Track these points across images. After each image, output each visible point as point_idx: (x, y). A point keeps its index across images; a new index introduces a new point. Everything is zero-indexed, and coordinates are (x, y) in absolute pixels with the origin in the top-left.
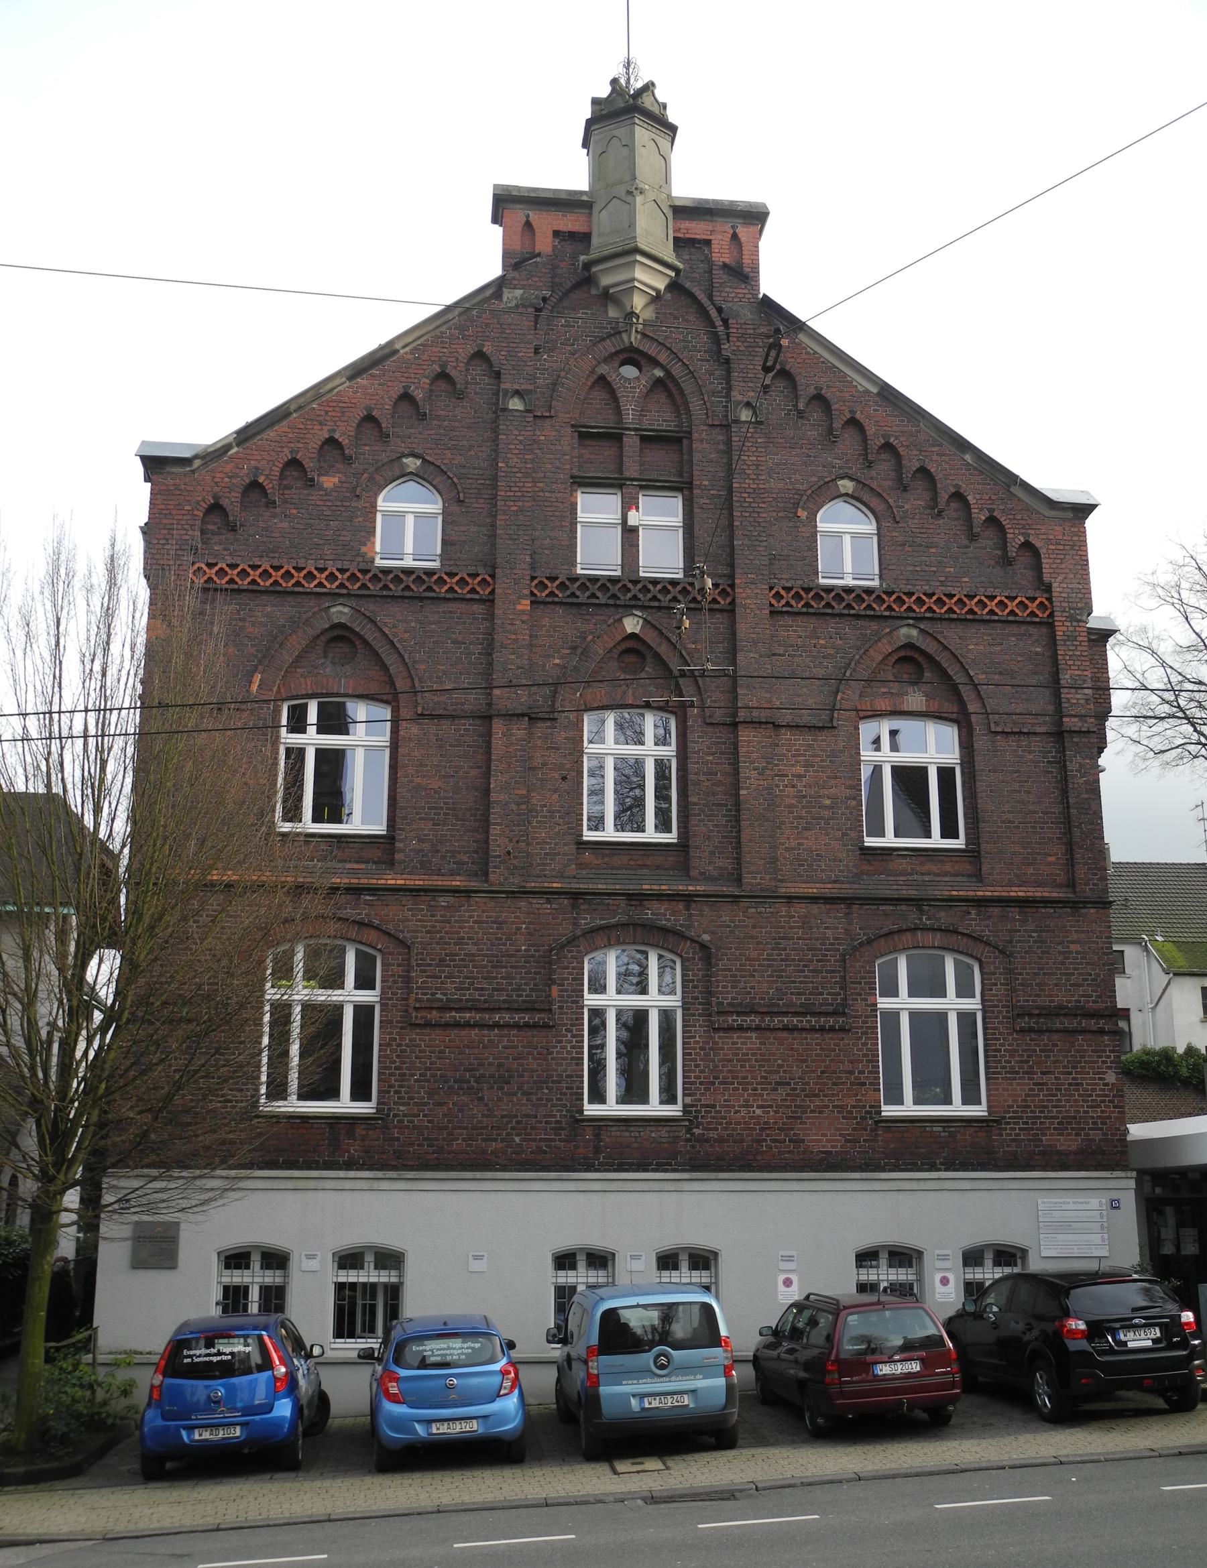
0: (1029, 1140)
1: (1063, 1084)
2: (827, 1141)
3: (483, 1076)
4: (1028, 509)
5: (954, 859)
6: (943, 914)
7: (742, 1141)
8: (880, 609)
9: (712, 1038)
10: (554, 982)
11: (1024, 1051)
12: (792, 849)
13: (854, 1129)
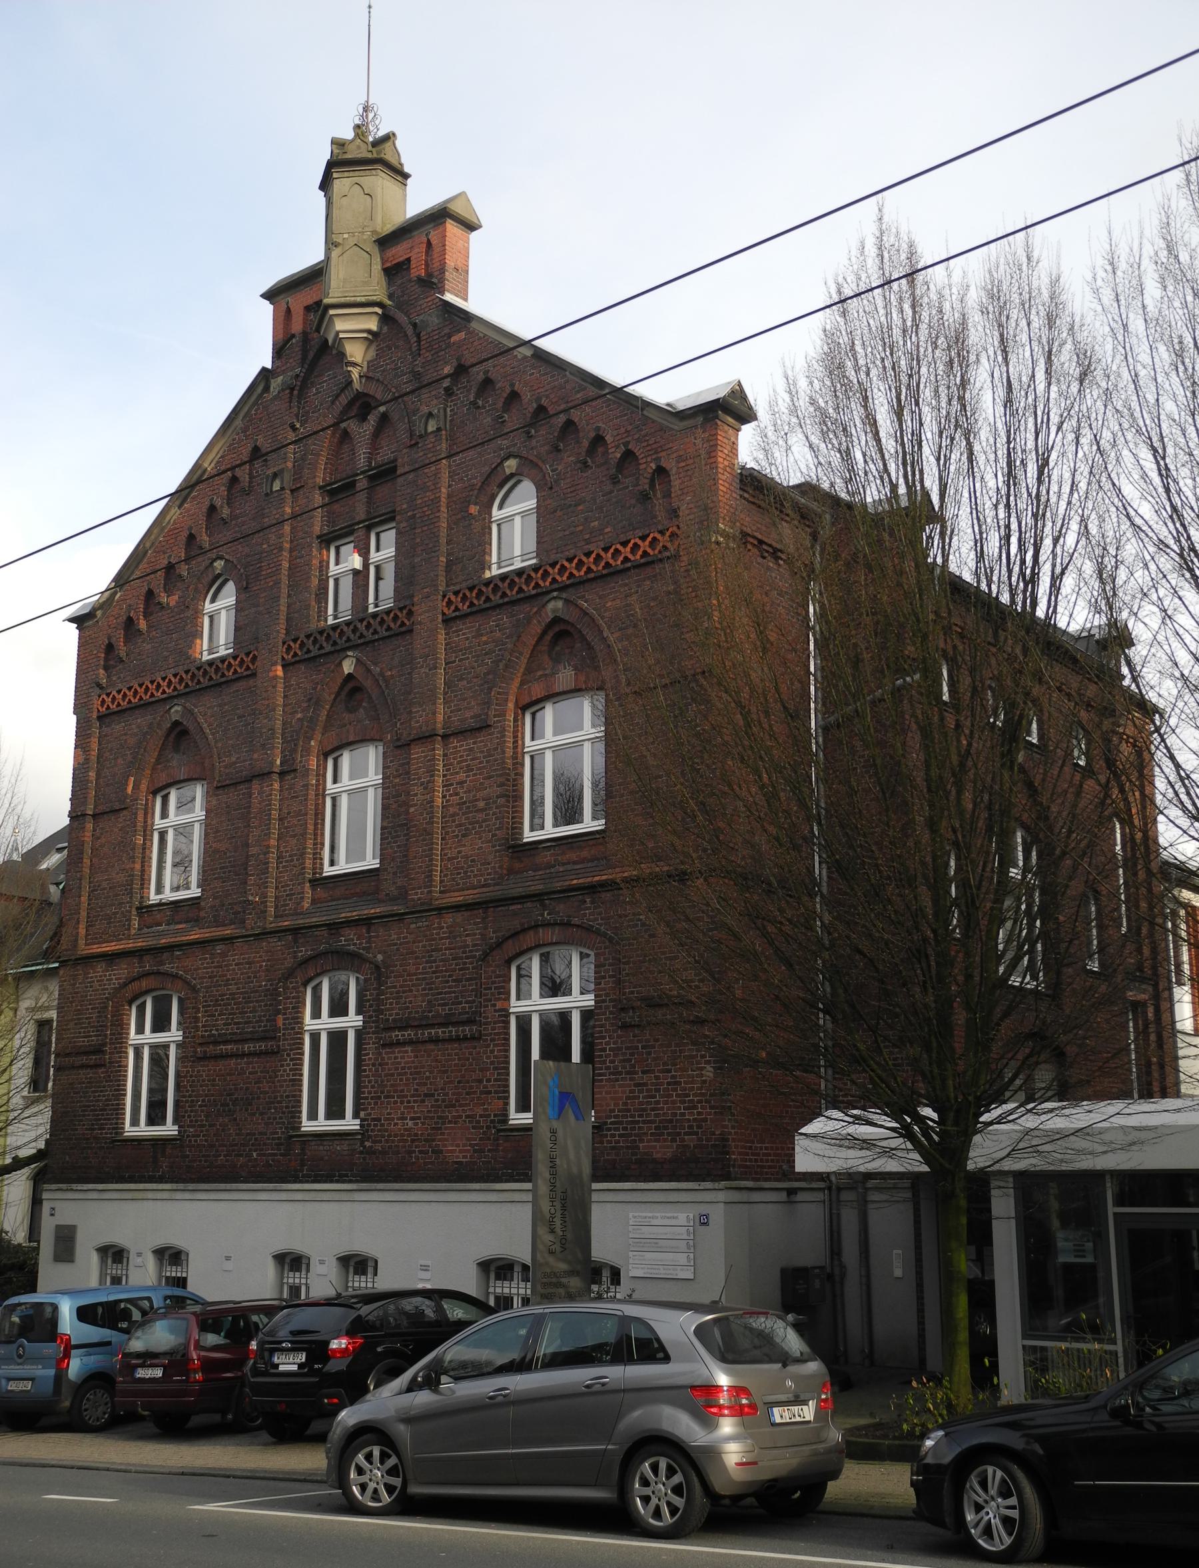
0: (627, 1147)
1: (662, 1084)
2: (460, 1151)
3: (236, 1099)
4: (662, 429)
5: (591, 843)
6: (562, 906)
7: (398, 1153)
8: (529, 590)
9: (380, 1054)
10: (278, 1012)
11: (627, 1048)
12: (454, 858)
13: (481, 1139)
